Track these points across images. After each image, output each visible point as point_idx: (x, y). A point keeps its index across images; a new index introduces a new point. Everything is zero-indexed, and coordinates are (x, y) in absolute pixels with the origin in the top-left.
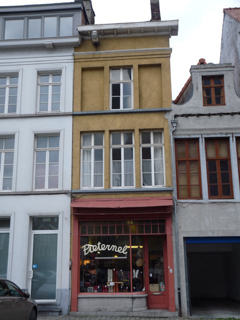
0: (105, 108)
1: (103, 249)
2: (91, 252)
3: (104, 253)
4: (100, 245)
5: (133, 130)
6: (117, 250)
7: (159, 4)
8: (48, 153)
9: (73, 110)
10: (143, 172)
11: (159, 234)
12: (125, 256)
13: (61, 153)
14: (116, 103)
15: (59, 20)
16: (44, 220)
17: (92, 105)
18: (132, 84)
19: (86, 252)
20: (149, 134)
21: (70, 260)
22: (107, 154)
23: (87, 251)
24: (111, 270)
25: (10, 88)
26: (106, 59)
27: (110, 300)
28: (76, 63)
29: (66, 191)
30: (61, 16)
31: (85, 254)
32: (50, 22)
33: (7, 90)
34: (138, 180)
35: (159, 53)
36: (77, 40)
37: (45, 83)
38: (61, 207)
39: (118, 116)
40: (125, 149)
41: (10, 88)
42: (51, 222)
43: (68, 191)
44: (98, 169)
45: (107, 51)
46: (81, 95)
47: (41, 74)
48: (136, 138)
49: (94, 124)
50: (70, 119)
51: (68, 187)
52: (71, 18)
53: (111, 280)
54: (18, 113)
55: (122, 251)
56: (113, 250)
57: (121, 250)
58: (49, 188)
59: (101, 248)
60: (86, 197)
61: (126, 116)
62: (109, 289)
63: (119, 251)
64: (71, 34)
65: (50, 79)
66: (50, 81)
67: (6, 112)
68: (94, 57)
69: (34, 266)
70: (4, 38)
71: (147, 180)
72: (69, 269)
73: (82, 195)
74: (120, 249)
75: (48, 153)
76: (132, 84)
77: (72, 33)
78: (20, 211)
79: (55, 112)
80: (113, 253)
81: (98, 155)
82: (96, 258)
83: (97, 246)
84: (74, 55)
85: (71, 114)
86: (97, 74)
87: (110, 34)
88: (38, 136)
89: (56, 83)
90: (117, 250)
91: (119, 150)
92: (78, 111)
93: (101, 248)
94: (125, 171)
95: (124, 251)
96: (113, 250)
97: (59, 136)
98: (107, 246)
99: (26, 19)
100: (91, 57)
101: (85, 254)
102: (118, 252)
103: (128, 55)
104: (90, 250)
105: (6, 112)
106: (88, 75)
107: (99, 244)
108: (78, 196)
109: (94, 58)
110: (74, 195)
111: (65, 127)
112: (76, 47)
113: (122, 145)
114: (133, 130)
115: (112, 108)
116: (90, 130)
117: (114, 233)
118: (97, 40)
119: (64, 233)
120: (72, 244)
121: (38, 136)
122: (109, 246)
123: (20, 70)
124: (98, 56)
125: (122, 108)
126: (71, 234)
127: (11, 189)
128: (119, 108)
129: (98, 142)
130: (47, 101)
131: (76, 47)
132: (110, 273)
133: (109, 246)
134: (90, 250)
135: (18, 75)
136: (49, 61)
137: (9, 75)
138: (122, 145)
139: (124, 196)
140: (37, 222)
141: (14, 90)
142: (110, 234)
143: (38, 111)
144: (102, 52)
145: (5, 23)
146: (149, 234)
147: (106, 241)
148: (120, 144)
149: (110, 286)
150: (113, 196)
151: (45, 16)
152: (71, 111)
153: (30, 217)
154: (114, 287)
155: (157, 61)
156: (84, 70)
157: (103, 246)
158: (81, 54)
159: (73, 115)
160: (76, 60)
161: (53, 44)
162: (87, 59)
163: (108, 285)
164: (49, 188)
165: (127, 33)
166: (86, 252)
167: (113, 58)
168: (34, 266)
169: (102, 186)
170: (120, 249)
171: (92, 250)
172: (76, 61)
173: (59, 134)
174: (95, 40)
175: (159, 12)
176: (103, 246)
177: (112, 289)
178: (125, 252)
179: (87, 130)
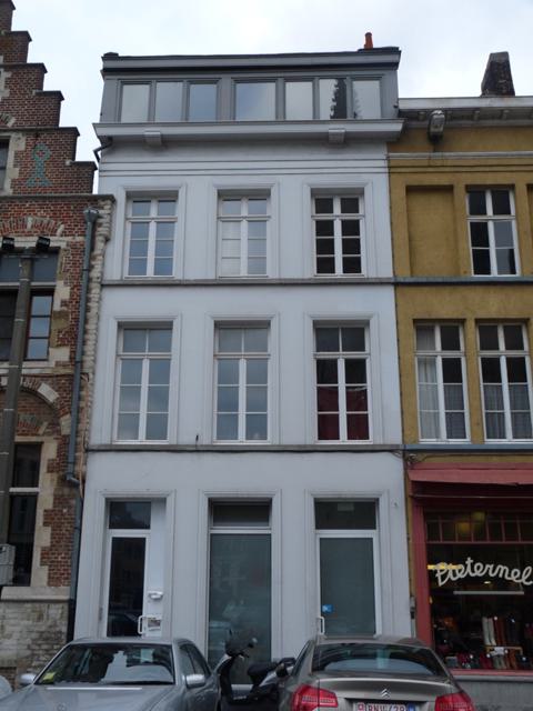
0: (462, 271)
1: (478, 573)
2: (472, 575)
3: (469, 582)
4: (472, 565)
5: (462, 321)
6: (509, 575)
7: (509, 66)
8: (146, 365)
9: (394, 272)
10: (486, 409)
11: (504, 542)
12: (519, 590)
13: (271, 366)
14: (482, 263)
15: (188, 89)
16: (340, 508)
17: (434, 263)
18: (514, 223)
19: (443, 580)
20: (495, 328)
21: (411, 596)
22: (471, 370)
23: (443, 577)
24: (491, 620)
25: (158, 223)
26: (457, 168)
27: (504, 686)
28: (393, 176)
29: (392, 445)
30: (192, 82)
31: (441, 584)
32: (169, 91)
33: (153, 227)
34: (476, 424)
35: (495, 162)
36: (397, 127)
37: (140, 218)
38: (380, 478)
39: (492, 289)
40: (509, 360)
41: (158, 223)
42: (363, 512)
43: (398, 445)
44: (454, 400)
45: (461, 153)
46: (407, 242)
47: (225, 195)
48: (470, 337)
49: (444, 305)
50: (389, 292)
51: (395, 438)
52: (212, 88)
53: (494, 643)
54: (177, 275)
55: (520, 578)
56: (501, 575)
57: (518, 575)
58: (147, 438)
59: (473, 571)
60: (436, 460)
61: (509, 291)
62: (497, 661)
63: (513, 578)
64: (377, 115)
65: (154, 210)
66: (244, 212)
67: (150, 273)
68: (432, 164)
69: (325, 608)
70: (119, 119)
71: (496, 429)
72: (409, 617)
73: (426, 455)
74: (516, 574)
75: (146, 365)
76: (514, 223)
77: (146, 117)
78: (294, 486)
79: (162, 278)
80: (501, 583)
81: (452, 371)
82: (456, 592)
83: (466, 566)
84: (388, 159)
85: (393, 281)
86: (436, 201)
87: (462, 118)
88: (222, 327)
89: (166, 217)
90: (509, 575)
91: (496, 361)
92: (405, 276)
93: (473, 571)
94: (513, 406)
95: (524, 578)
96: (501, 575)
97: (171, 329)
98: (487, 566)
99: (280, 81)
100: (427, 164)
101: (441, 584)
102: (477, 577)
103: (505, 162)
104: (450, 575)
105: (150, 273)
106: (420, 201)
107: (469, 561)
108: (419, 457)
109: (430, 167)
110: (410, 456)
111: (379, 309)
112: (393, 142)
113: (503, 353)
114: (462, 321)
115: (475, 273)
116: (433, 317)
117: (516, 539)
118: (441, 129)
119: (392, 544)
120: (412, 563)
121: (222, 327)
122: (491, 567)
123: (272, 185)
124: (439, 163)
125: (494, 273)
126: (408, 539)
127: (136, 438)
128: (489, 273)
129: (451, 342)
130: (146, 254)
131: (393, 142)
132: (488, 626)
133: (491, 567)
134: (450, 575)
135: (177, 196)
136: (244, 169)
137: (155, 197)
138: (503, 353)
139: (519, 459)
140: (329, 512)
141: (166, 225)
142: (507, 540)
143: (126, 275)
144: (450, 156)
145: (122, 88)
146: (437, 542)
147: (482, 555)
148: (497, 348)
149: (498, 656)
150: (495, 460)
151: (159, 81)
152: (391, 275)
153: (107, 499)
154: (507, 657)
155: (443, 180)
156: (411, 190)
157: (478, 568)
158: (402, 156)
159: (397, 284)
160: (392, 170)
161: (162, 135)
162: (416, 168)
163: (494, 653)
164: (147, 438)
165: (500, 117)
166: (443, 580)
167: (472, 168)
168: (325, 608)
169: (465, 437)
170: (516, 574)
171: (455, 575)
172: (393, 170)
173: (171, 324)
174: (436, 130)
175: (510, 79)
176: (478, 568)
177: (503, 662)
178: (527, 580)
179: (427, 317)
